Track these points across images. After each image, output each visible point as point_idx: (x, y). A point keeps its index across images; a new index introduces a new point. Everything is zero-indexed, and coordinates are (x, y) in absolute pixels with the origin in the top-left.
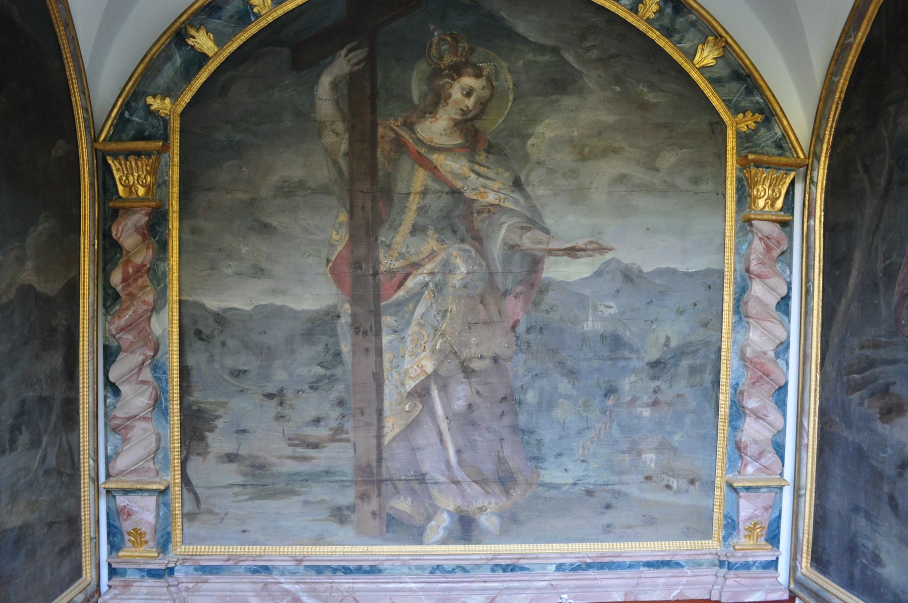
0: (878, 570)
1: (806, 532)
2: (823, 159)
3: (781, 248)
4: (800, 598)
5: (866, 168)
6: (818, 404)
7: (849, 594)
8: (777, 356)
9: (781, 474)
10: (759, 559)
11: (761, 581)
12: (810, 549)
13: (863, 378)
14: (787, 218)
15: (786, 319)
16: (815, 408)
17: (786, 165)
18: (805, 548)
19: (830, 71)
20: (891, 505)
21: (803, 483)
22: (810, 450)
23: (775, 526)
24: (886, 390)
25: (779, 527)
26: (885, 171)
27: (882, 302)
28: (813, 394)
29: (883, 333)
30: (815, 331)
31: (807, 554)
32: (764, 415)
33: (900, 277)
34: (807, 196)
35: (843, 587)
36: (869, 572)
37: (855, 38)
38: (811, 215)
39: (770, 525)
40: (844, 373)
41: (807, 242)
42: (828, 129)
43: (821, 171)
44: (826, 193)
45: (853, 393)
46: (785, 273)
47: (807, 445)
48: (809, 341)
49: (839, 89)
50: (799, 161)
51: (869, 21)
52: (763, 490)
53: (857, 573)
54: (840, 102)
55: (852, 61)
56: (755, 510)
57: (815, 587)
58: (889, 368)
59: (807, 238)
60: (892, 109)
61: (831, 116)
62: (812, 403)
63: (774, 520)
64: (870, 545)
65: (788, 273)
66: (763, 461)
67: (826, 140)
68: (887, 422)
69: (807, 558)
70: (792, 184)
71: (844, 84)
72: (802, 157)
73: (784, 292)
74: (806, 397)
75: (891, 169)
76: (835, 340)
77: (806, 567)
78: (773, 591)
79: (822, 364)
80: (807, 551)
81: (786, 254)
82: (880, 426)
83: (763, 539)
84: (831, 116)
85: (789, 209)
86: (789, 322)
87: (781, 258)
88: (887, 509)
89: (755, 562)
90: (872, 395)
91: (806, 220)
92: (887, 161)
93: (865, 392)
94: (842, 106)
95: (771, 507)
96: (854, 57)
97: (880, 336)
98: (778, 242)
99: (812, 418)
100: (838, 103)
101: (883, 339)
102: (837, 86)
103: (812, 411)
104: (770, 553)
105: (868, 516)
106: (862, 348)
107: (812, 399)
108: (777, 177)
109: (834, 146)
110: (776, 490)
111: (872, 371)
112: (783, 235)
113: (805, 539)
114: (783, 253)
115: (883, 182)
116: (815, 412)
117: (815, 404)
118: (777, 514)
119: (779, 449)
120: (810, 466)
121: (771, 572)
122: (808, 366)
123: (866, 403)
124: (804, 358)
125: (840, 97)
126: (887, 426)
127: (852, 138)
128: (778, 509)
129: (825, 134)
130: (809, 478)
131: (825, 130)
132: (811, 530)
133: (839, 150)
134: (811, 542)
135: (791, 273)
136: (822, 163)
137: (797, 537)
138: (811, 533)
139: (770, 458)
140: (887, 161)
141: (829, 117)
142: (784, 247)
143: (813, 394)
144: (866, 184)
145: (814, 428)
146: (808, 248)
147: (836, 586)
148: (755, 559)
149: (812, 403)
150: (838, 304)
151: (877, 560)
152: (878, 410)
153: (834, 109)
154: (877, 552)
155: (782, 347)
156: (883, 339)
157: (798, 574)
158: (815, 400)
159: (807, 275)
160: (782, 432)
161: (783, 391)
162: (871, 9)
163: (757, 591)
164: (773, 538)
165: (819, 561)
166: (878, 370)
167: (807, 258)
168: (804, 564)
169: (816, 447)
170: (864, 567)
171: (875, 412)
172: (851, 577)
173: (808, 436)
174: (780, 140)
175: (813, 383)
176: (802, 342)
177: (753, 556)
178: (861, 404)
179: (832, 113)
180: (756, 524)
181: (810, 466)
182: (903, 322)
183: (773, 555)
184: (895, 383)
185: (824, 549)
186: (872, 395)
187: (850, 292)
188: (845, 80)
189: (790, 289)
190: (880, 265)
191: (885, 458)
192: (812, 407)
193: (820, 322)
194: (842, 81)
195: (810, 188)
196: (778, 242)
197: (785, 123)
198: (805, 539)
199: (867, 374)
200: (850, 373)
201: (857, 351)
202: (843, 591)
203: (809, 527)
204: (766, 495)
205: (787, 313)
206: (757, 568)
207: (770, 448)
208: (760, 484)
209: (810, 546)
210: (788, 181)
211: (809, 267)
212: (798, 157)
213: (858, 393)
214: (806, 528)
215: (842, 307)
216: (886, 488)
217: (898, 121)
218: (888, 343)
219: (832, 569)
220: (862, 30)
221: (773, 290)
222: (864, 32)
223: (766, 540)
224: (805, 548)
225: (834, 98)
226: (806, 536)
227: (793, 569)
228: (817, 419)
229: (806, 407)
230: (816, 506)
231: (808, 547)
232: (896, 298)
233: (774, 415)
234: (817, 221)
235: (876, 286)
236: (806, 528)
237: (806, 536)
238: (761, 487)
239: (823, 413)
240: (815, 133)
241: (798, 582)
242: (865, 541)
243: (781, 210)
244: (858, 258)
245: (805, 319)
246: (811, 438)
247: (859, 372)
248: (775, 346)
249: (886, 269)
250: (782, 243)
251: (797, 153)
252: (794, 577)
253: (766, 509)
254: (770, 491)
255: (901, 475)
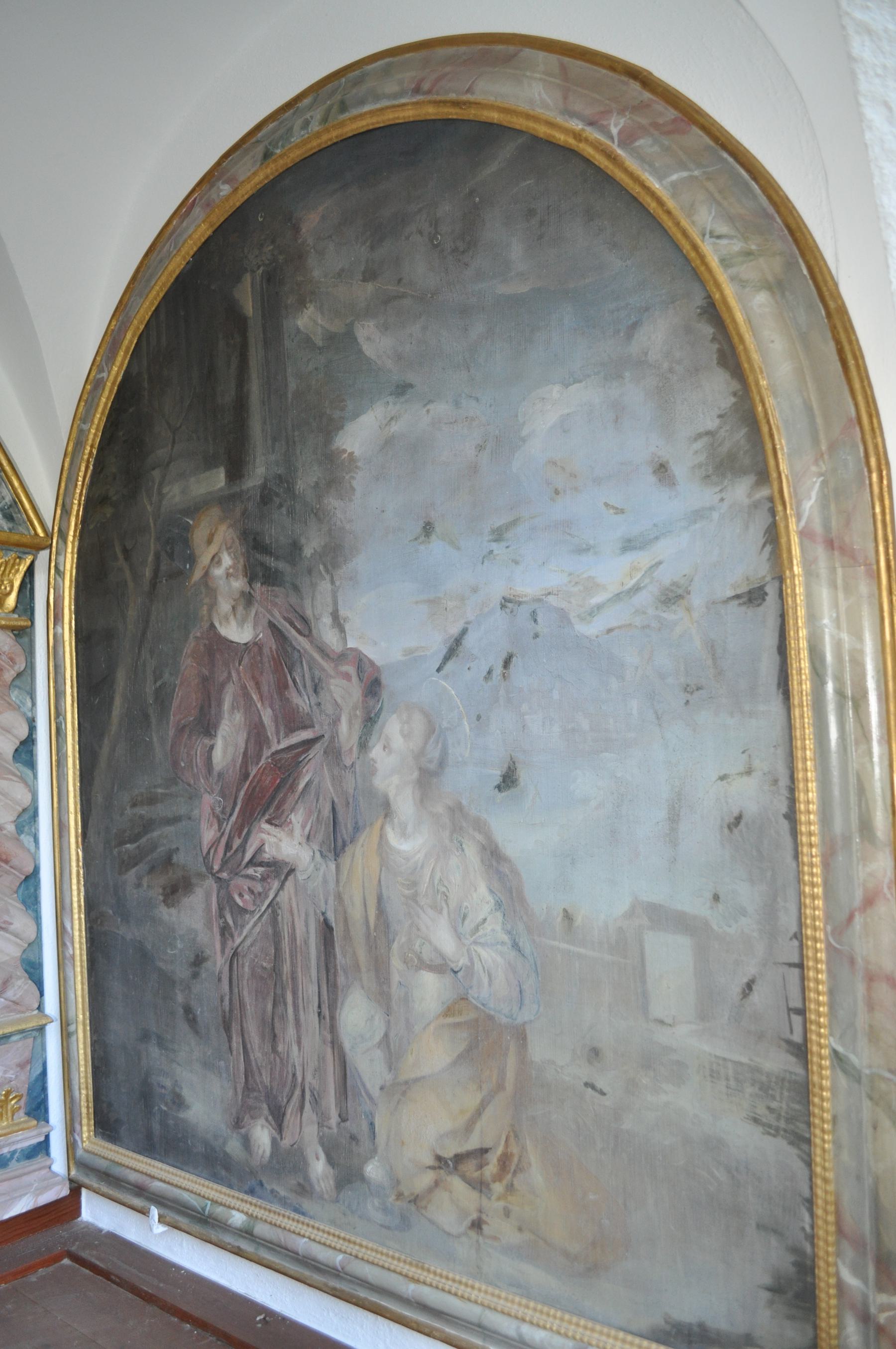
0: (182, 1115)
1: (83, 1086)
2: (70, 538)
3: (16, 668)
4: (87, 1188)
5: (126, 552)
6: (82, 894)
7: (149, 1160)
8: (20, 829)
9: (40, 1008)
10: (19, 1146)
11: (26, 1179)
12: (91, 1110)
13: (138, 847)
14: (22, 623)
15: (29, 772)
16: (79, 901)
17: (18, 545)
18: (84, 1110)
19: (79, 416)
20: (188, 1020)
21: (71, 1014)
22: (78, 963)
23: (38, 1088)
24: (168, 861)
25: (44, 1089)
26: (151, 558)
27: (155, 739)
28: (74, 881)
29: (160, 781)
30: (71, 788)
31: (89, 1119)
32: (5, 922)
33: (175, 703)
34: (52, 591)
35: (139, 1153)
36: (171, 1122)
37: (109, 372)
38: (58, 618)
39: (30, 1090)
40: (113, 843)
41: (55, 658)
42: (77, 496)
43: (69, 556)
44: (77, 588)
45: (127, 870)
46: (24, 704)
47: (73, 957)
48: (64, 803)
49: (90, 442)
50: (36, 541)
51: (126, 352)
52: (14, 1038)
53: (156, 1127)
54: (92, 461)
55: (106, 404)
56: (5, 1072)
57: (102, 1164)
58: (169, 830)
59: (54, 652)
60: (156, 474)
61: (80, 479)
62: (75, 893)
63: (37, 1080)
64: (168, 1083)
65: (29, 704)
66: (10, 994)
67: (74, 512)
68: (173, 906)
69: (88, 1125)
70: (30, 571)
71: (95, 435)
72: (42, 534)
73: (24, 733)
74: (66, 886)
75: (157, 557)
76: (98, 798)
77: (89, 1138)
78: (46, 1188)
79: (84, 834)
80: (88, 1114)
81: (27, 674)
82: (165, 913)
83: (21, 1113)
84: (80, 479)
85: (25, 611)
86: (35, 776)
87: (17, 682)
88: (183, 1027)
89: (14, 1152)
90: (152, 870)
91: (51, 626)
92: (152, 546)
93: (142, 867)
94: (94, 466)
95: (29, 1061)
96: (108, 399)
97: (155, 787)
98: (12, 659)
99: (76, 916)
100: (88, 461)
101: (160, 791)
102: (87, 436)
103: (75, 905)
104: (34, 1133)
105: (161, 1043)
106: (134, 805)
107: (74, 887)
108: (7, 563)
109: (85, 522)
110: (35, 1033)
111: (148, 836)
112: (18, 649)
113: (83, 1096)
114: (19, 675)
115: (148, 573)
116: (80, 906)
117: (79, 894)
118: (39, 1070)
119: (33, 970)
120: (79, 987)
121: (40, 1160)
122: (65, 839)
123: (145, 882)
124: (61, 828)
125: (91, 453)
126: (173, 911)
127: (109, 511)
128: (40, 1062)
129: (72, 503)
130: (80, 1006)
131: (73, 498)
132: (90, 1081)
133: (91, 527)
134: (91, 1099)
135: (34, 704)
136: (70, 545)
137: (72, 1097)
138: (91, 1086)
139: (22, 987)
140: (152, 546)
141: (77, 480)
142: (21, 666)
143: (74, 881)
144: (128, 574)
145: (80, 930)
146: (56, 667)
147: (131, 1154)
148: (13, 1148)
149: (75, 893)
150: (100, 747)
151: (179, 1102)
152: (161, 891)
153: (83, 469)
154: (177, 1090)
155: (26, 816)
156: (160, 791)
157: (80, 1152)
158: (79, 889)
159: (56, 708)
160: (36, 943)
161: (32, 881)
162: (129, 336)
163: (21, 1196)
164: (38, 1108)
165: (105, 1126)
166: (155, 834)
167: (56, 682)
168: (85, 1135)
169: (85, 957)
170: (165, 1115)
171: (156, 893)
172: (149, 1136)
173: (73, 943)
174: (11, 506)
175: (74, 864)
176: (56, 805)
177: (9, 1144)
178: (139, 885)
179: (81, 474)
180: (8, 1093)
181: (79, 987)
182: (183, 765)
183: (39, 1135)
184: (178, 849)
185: (110, 1105)
186: (152, 870)
187: (114, 728)
188: (97, 430)
189: (32, 728)
190: (150, 689)
191: (175, 954)
192: (75, 899)
193: (78, 773)
194: (93, 431)
195: (55, 579)
196: (12, 659)
197: (16, 484)
198: (83, 1096)
199: (143, 840)
200: (121, 843)
201: (129, 811)
202: (141, 1158)
203: (86, 1077)
204: (20, 1044)
205: (31, 764)
206: (18, 1160)
207: (20, 972)
208: (8, 1030)
209: (91, 1105)
210: (23, 568)
211: (59, 695)
212: (36, 534)
213: (134, 870)
214: (82, 1080)
215: (105, 750)
216: (180, 998)
217: (165, 491)
218: (166, 795)
219: (123, 1131)
220: (118, 363)
221: (8, 731)
222: (102, 413)
223: (28, 1114)
224: (84, 1110)
225: (83, 454)
226: (84, 1092)
227: (71, 1146)
228: (83, 916)
229: (67, 901)
230: (93, 1044)
231: (88, 1107)
232: (171, 732)
233: (21, 922)
234: (66, 627)
235: (146, 716)
236: (82, 1080)
237: (84, 1092)
238: (10, 1035)
239: (90, 906)
240: (60, 501)
241: (83, 1165)
242: (161, 1078)
243: (14, 611)
244: (121, 677)
245: (58, 771)
246: (77, 946)
247: (131, 841)
248: (16, 815)
249: (158, 691)
250: (17, 660)
251: (34, 529)
252: (74, 1158)
253: (22, 1066)
254: (25, 1038)
255: (195, 975)
